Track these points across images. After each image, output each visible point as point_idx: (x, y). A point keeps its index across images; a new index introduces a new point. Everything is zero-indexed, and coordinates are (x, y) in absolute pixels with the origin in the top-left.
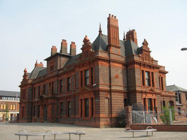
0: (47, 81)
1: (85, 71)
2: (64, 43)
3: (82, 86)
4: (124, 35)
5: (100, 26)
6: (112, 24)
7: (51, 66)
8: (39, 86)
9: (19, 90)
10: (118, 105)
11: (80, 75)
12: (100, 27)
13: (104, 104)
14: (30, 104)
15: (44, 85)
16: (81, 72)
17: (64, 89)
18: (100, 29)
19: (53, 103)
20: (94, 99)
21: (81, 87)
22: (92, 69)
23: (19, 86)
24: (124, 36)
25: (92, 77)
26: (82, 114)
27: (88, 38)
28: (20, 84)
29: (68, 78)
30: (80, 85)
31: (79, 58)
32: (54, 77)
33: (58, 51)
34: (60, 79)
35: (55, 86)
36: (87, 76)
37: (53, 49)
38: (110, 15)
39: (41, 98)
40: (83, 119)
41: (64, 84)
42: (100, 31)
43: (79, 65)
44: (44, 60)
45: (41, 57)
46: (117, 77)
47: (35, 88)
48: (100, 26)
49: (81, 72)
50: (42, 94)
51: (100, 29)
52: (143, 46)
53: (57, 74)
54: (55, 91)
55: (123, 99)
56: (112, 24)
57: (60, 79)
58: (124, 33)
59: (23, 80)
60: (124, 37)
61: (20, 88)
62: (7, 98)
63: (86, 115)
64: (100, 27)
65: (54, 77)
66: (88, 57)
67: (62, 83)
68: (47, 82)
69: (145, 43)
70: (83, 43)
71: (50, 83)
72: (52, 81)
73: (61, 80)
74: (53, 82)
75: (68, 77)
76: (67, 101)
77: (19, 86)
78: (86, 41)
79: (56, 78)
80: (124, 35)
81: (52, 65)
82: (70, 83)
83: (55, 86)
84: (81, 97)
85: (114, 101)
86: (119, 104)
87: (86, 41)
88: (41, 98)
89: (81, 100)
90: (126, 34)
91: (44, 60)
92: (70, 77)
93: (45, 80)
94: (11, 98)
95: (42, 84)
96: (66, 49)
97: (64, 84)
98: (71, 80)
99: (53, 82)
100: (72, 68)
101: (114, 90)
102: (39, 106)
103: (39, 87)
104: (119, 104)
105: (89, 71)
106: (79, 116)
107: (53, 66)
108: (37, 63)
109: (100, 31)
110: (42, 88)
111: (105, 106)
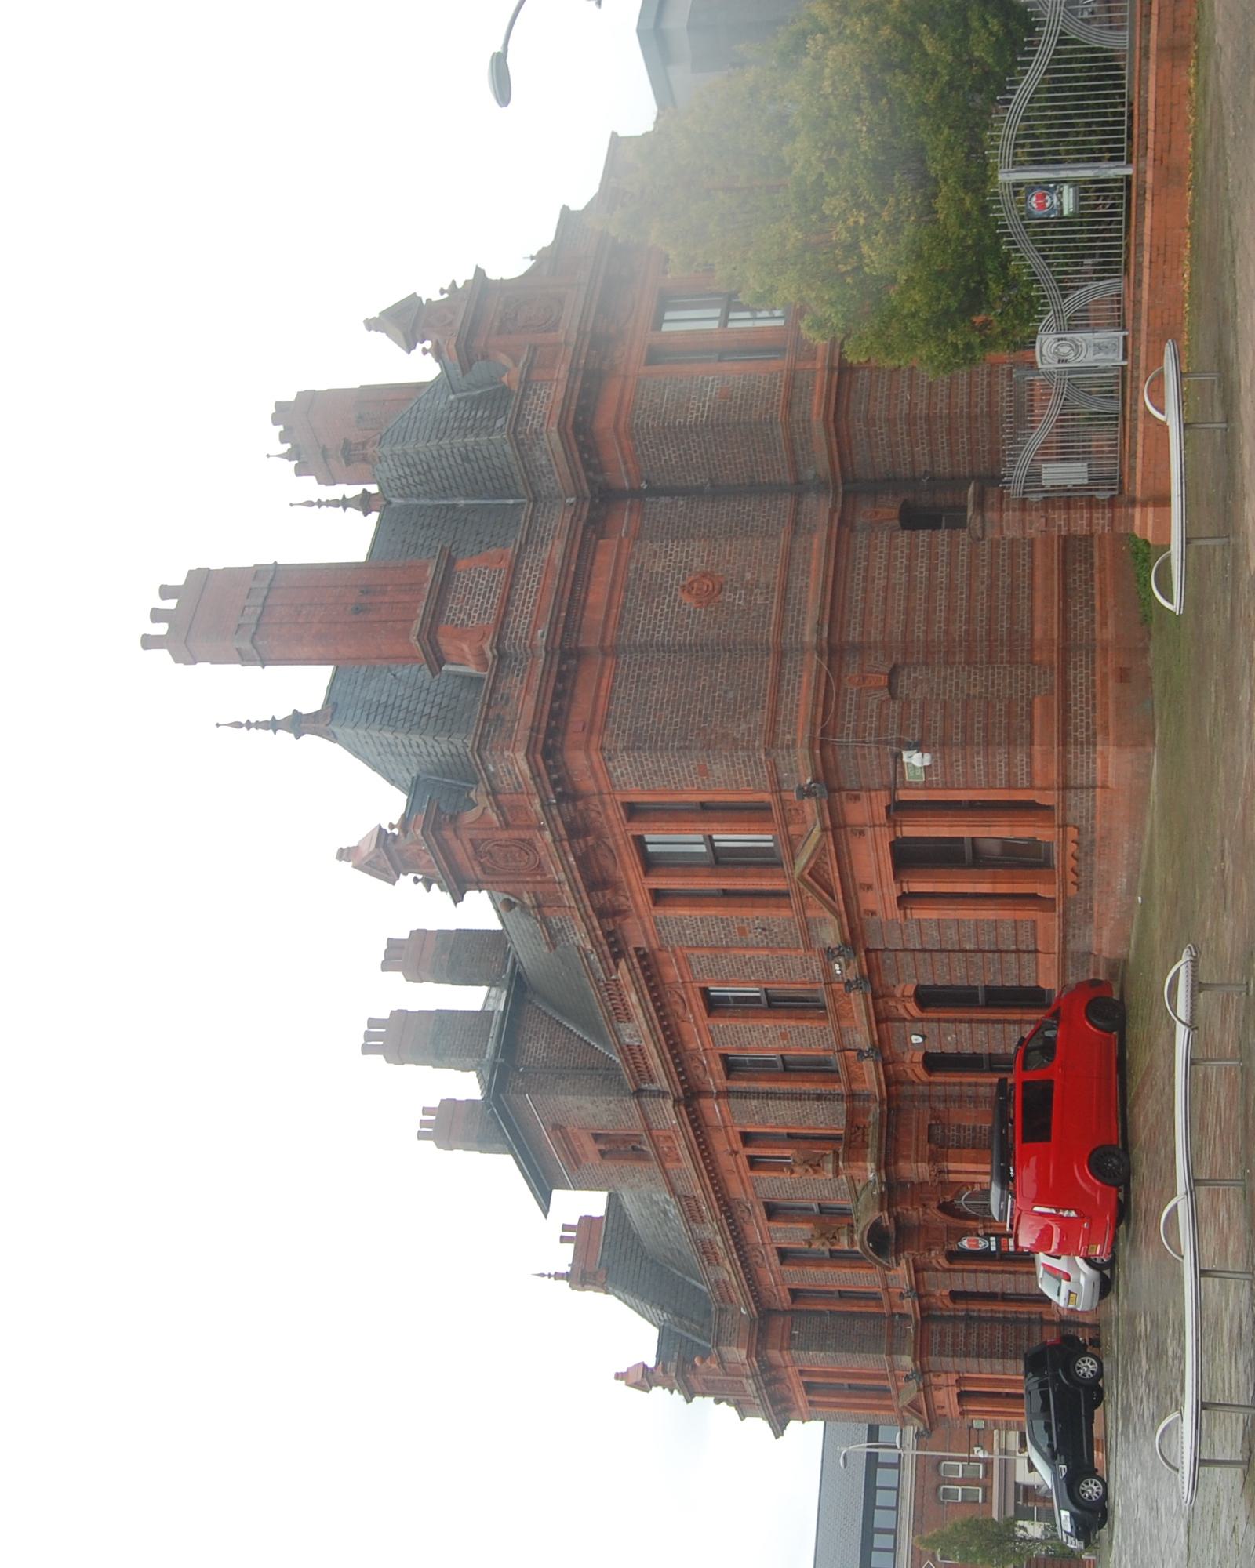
0: (736, 1190)
1: (650, 863)
2: (404, 1038)
3: (785, 895)
4: (328, 503)
5: (249, 725)
6: (226, 615)
7: (603, 1154)
8: (760, 1211)
9: (806, 1436)
10: (951, 588)
11: (684, 912)
12: (259, 725)
13: (945, 706)
14: (937, 1339)
15: (773, 1211)
16: (659, 897)
17: (804, 1038)
18: (273, 725)
19: (930, 1139)
20: (903, 795)
21: (794, 900)
22: (633, 811)
23: (778, 1430)
24: (335, 503)
25: (707, 810)
26: (1033, 897)
27: (357, 832)
28: (759, 1426)
29: (714, 1005)
30: (779, 917)
31: (545, 921)
32: (698, 1124)
33: (465, 1085)
34: (715, 1080)
35: (779, 1116)
36: (702, 849)
37: (448, 1126)
38: (148, 642)
39: (881, 1242)
40: (1072, 890)
41: (763, 1039)
42: (298, 724)
43: (602, 913)
44: (546, 1213)
45: (507, 1226)
46: (708, 588)
47: (795, 1294)
48: (249, 725)
49: (659, 897)
50: (851, 1232)
51: (273, 725)
52: (428, 344)
53: (677, 1102)
54: (827, 1118)
55: (903, 537)
56: (226, 615)
57: (715, 1080)
58: (310, 504)
59: (718, 1401)
60: (344, 503)
61: (794, 1426)
62: (879, 1541)
63: (1027, 859)
64: (259, 725)
65: (698, 1124)
66: (531, 843)
67: (731, 991)
68: (753, 1190)
69: (407, 322)
70: (406, 880)
71: (753, 1162)
72: (738, 1145)
73: (731, 1067)
74: (747, 1138)
75: (698, 1004)
76: (915, 1020)
77: (778, 1430)
78: (384, 857)
79: (714, 1110)
80: (328, 503)
81: (591, 1148)
82: (752, 991)
83: (779, 1116)
84: (880, 894)
85: (943, 550)
86: (943, 572)
87: (384, 857)
88: (881, 1242)
89: (905, 900)
90: (310, 487)
91: (546, 1213)
92: (705, 991)
93: (727, 1206)
94: (883, 1498)
95: (758, 1229)
96: (445, 1020)
97: (763, 1039)
98: (726, 982)
99: (801, 1372)
100: (623, 973)
101: (824, 596)
102: (952, 1256)
103: (784, 1255)
104: (943, 572)
105: (654, 831)
106: (1049, 924)
107: (597, 1137)
108: (558, 1276)
109: (298, 724)
110: (796, 1234)
111: (966, 705)
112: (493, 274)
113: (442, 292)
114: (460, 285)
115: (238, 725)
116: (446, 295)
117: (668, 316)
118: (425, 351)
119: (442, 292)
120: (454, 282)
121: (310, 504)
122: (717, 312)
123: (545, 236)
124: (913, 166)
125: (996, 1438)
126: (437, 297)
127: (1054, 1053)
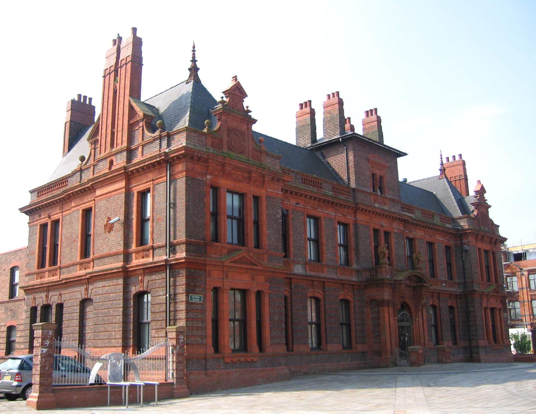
4: (442, 160)
5: (194, 51)
18: (194, 61)
48: (194, 51)
51: (194, 61)
80: (442, 160)
112: (489, 210)
113: (247, 107)
114: (249, 114)
115: (194, 47)
116: (246, 109)
117: (312, 220)
118: (222, 98)
119: (247, 107)
120: (250, 112)
121: (441, 156)
122: (313, 237)
123: (496, 223)
124: (472, 309)
125: (310, 329)
126: (245, 104)
127: (8, 355)
